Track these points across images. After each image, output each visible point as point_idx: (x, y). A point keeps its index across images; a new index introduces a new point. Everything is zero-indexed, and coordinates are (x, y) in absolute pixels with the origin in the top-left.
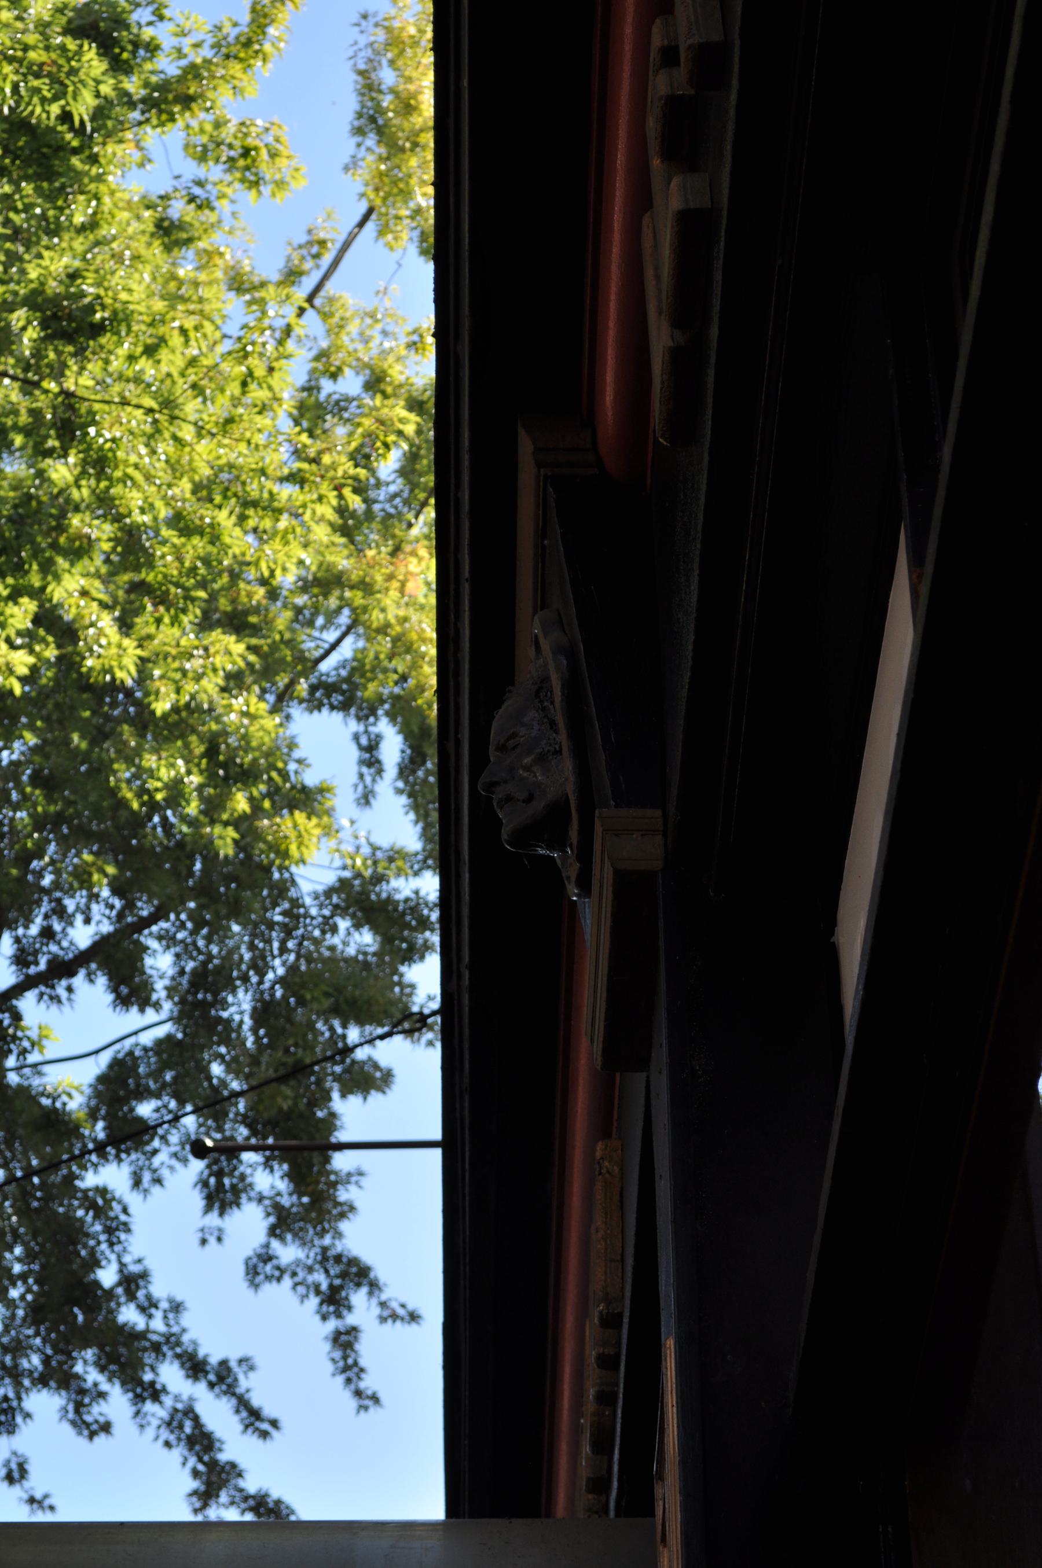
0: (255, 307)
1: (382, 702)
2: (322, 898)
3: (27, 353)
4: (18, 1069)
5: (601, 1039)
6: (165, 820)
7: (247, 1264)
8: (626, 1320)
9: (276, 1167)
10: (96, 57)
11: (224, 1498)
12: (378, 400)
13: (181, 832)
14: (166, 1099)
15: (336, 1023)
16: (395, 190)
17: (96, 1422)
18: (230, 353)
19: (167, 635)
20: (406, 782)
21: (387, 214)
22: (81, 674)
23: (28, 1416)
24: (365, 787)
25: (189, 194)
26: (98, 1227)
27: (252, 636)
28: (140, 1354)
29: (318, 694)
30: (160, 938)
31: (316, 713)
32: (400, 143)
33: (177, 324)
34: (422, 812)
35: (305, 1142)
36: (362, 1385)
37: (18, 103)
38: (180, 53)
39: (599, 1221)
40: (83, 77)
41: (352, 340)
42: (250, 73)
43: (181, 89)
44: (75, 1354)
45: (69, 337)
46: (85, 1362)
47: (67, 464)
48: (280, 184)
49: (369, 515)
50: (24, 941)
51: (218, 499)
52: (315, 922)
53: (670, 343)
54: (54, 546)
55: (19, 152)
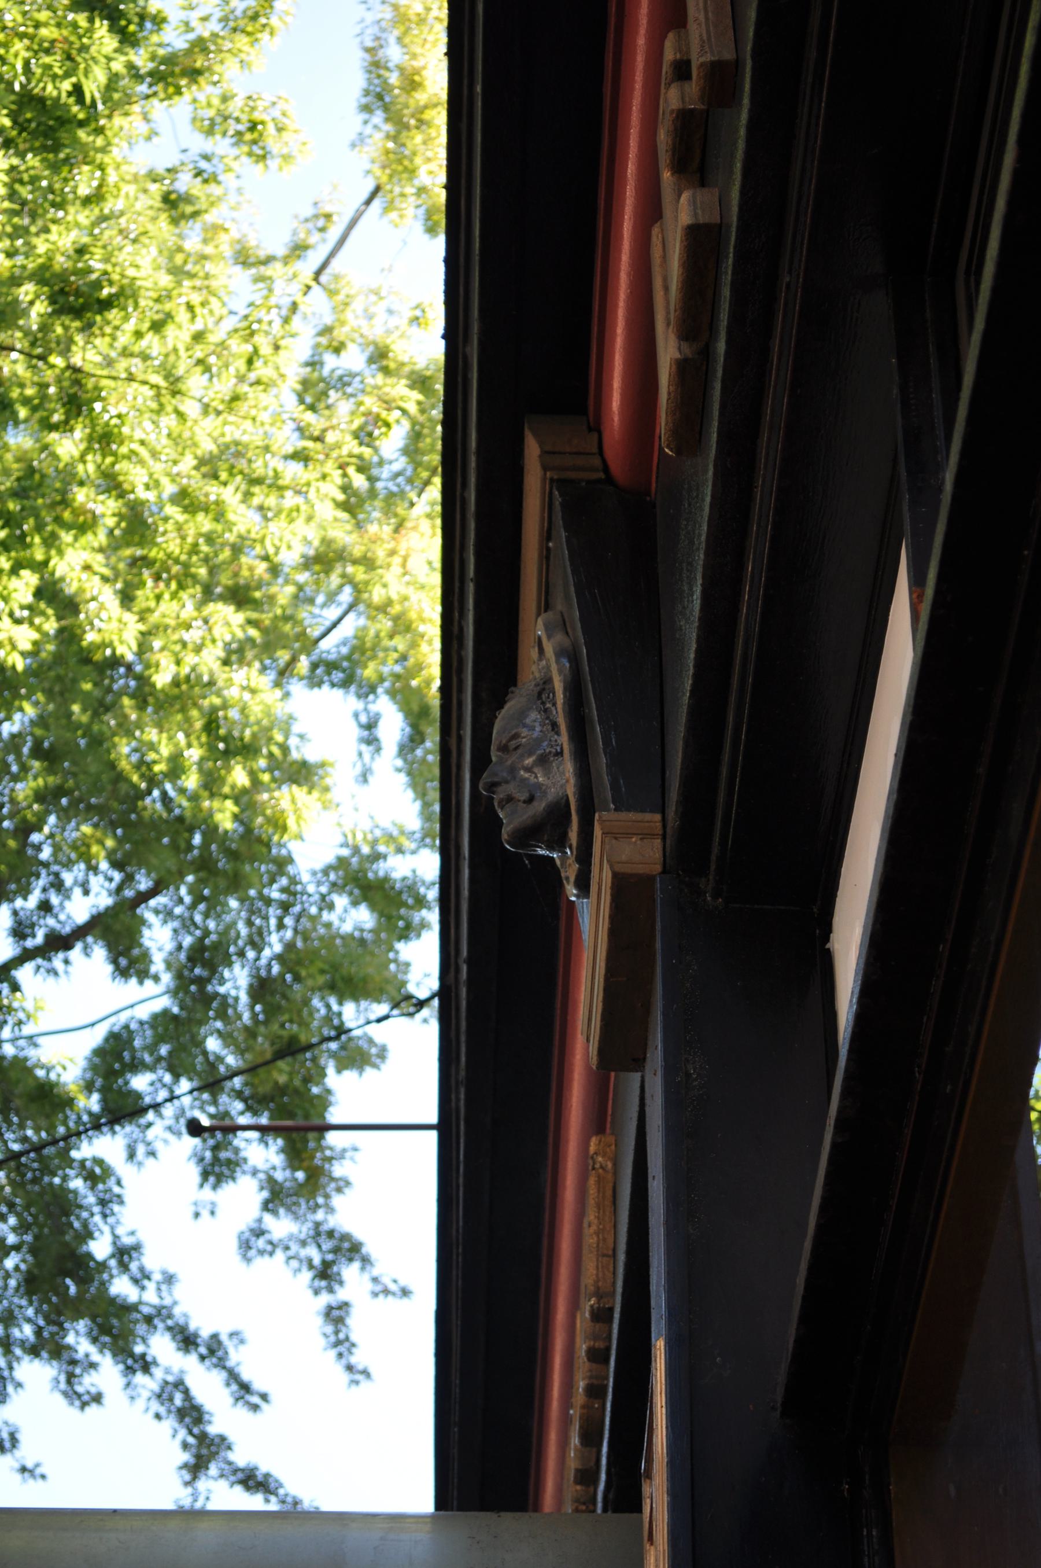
0: (261, 285)
1: (382, 679)
2: (319, 875)
3: (35, 327)
4: (13, 1041)
5: (597, 1038)
6: (164, 794)
7: (239, 1237)
8: (617, 1316)
9: (271, 1142)
10: (107, 34)
11: (213, 1470)
12: (380, 379)
13: (180, 806)
14: (160, 1072)
15: (333, 1001)
16: (400, 168)
17: (88, 1392)
18: (236, 331)
19: (167, 609)
20: (405, 760)
21: (391, 192)
22: (81, 649)
23: (19, 1385)
24: (364, 765)
25: (195, 168)
26: (91, 1199)
27: (255, 610)
28: (131, 1325)
29: (319, 671)
30: (157, 912)
31: (316, 690)
32: (405, 119)
33: (183, 300)
34: (419, 789)
35: (300, 1122)
36: (353, 1360)
37: (29, 81)
38: (188, 27)
39: (591, 1216)
40: (95, 55)
41: (356, 317)
42: (257, 46)
43: (187, 62)
44: (67, 1325)
45: (77, 312)
46: (77, 1333)
47: (73, 440)
48: (287, 158)
49: (372, 493)
50: (21, 913)
51: (224, 476)
52: (312, 899)
53: (678, 355)
54: (58, 520)
55: (26, 125)
